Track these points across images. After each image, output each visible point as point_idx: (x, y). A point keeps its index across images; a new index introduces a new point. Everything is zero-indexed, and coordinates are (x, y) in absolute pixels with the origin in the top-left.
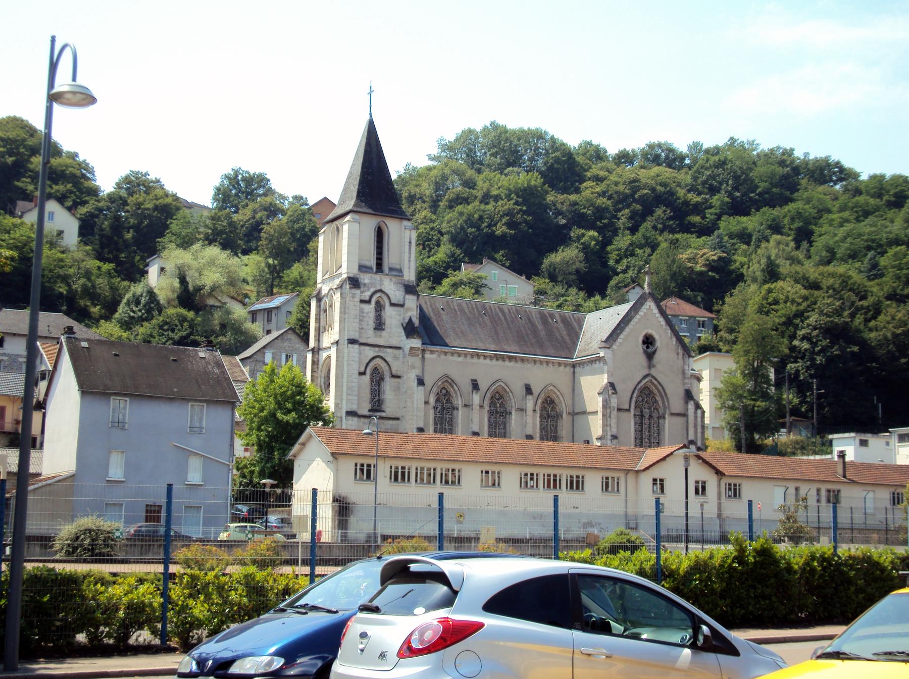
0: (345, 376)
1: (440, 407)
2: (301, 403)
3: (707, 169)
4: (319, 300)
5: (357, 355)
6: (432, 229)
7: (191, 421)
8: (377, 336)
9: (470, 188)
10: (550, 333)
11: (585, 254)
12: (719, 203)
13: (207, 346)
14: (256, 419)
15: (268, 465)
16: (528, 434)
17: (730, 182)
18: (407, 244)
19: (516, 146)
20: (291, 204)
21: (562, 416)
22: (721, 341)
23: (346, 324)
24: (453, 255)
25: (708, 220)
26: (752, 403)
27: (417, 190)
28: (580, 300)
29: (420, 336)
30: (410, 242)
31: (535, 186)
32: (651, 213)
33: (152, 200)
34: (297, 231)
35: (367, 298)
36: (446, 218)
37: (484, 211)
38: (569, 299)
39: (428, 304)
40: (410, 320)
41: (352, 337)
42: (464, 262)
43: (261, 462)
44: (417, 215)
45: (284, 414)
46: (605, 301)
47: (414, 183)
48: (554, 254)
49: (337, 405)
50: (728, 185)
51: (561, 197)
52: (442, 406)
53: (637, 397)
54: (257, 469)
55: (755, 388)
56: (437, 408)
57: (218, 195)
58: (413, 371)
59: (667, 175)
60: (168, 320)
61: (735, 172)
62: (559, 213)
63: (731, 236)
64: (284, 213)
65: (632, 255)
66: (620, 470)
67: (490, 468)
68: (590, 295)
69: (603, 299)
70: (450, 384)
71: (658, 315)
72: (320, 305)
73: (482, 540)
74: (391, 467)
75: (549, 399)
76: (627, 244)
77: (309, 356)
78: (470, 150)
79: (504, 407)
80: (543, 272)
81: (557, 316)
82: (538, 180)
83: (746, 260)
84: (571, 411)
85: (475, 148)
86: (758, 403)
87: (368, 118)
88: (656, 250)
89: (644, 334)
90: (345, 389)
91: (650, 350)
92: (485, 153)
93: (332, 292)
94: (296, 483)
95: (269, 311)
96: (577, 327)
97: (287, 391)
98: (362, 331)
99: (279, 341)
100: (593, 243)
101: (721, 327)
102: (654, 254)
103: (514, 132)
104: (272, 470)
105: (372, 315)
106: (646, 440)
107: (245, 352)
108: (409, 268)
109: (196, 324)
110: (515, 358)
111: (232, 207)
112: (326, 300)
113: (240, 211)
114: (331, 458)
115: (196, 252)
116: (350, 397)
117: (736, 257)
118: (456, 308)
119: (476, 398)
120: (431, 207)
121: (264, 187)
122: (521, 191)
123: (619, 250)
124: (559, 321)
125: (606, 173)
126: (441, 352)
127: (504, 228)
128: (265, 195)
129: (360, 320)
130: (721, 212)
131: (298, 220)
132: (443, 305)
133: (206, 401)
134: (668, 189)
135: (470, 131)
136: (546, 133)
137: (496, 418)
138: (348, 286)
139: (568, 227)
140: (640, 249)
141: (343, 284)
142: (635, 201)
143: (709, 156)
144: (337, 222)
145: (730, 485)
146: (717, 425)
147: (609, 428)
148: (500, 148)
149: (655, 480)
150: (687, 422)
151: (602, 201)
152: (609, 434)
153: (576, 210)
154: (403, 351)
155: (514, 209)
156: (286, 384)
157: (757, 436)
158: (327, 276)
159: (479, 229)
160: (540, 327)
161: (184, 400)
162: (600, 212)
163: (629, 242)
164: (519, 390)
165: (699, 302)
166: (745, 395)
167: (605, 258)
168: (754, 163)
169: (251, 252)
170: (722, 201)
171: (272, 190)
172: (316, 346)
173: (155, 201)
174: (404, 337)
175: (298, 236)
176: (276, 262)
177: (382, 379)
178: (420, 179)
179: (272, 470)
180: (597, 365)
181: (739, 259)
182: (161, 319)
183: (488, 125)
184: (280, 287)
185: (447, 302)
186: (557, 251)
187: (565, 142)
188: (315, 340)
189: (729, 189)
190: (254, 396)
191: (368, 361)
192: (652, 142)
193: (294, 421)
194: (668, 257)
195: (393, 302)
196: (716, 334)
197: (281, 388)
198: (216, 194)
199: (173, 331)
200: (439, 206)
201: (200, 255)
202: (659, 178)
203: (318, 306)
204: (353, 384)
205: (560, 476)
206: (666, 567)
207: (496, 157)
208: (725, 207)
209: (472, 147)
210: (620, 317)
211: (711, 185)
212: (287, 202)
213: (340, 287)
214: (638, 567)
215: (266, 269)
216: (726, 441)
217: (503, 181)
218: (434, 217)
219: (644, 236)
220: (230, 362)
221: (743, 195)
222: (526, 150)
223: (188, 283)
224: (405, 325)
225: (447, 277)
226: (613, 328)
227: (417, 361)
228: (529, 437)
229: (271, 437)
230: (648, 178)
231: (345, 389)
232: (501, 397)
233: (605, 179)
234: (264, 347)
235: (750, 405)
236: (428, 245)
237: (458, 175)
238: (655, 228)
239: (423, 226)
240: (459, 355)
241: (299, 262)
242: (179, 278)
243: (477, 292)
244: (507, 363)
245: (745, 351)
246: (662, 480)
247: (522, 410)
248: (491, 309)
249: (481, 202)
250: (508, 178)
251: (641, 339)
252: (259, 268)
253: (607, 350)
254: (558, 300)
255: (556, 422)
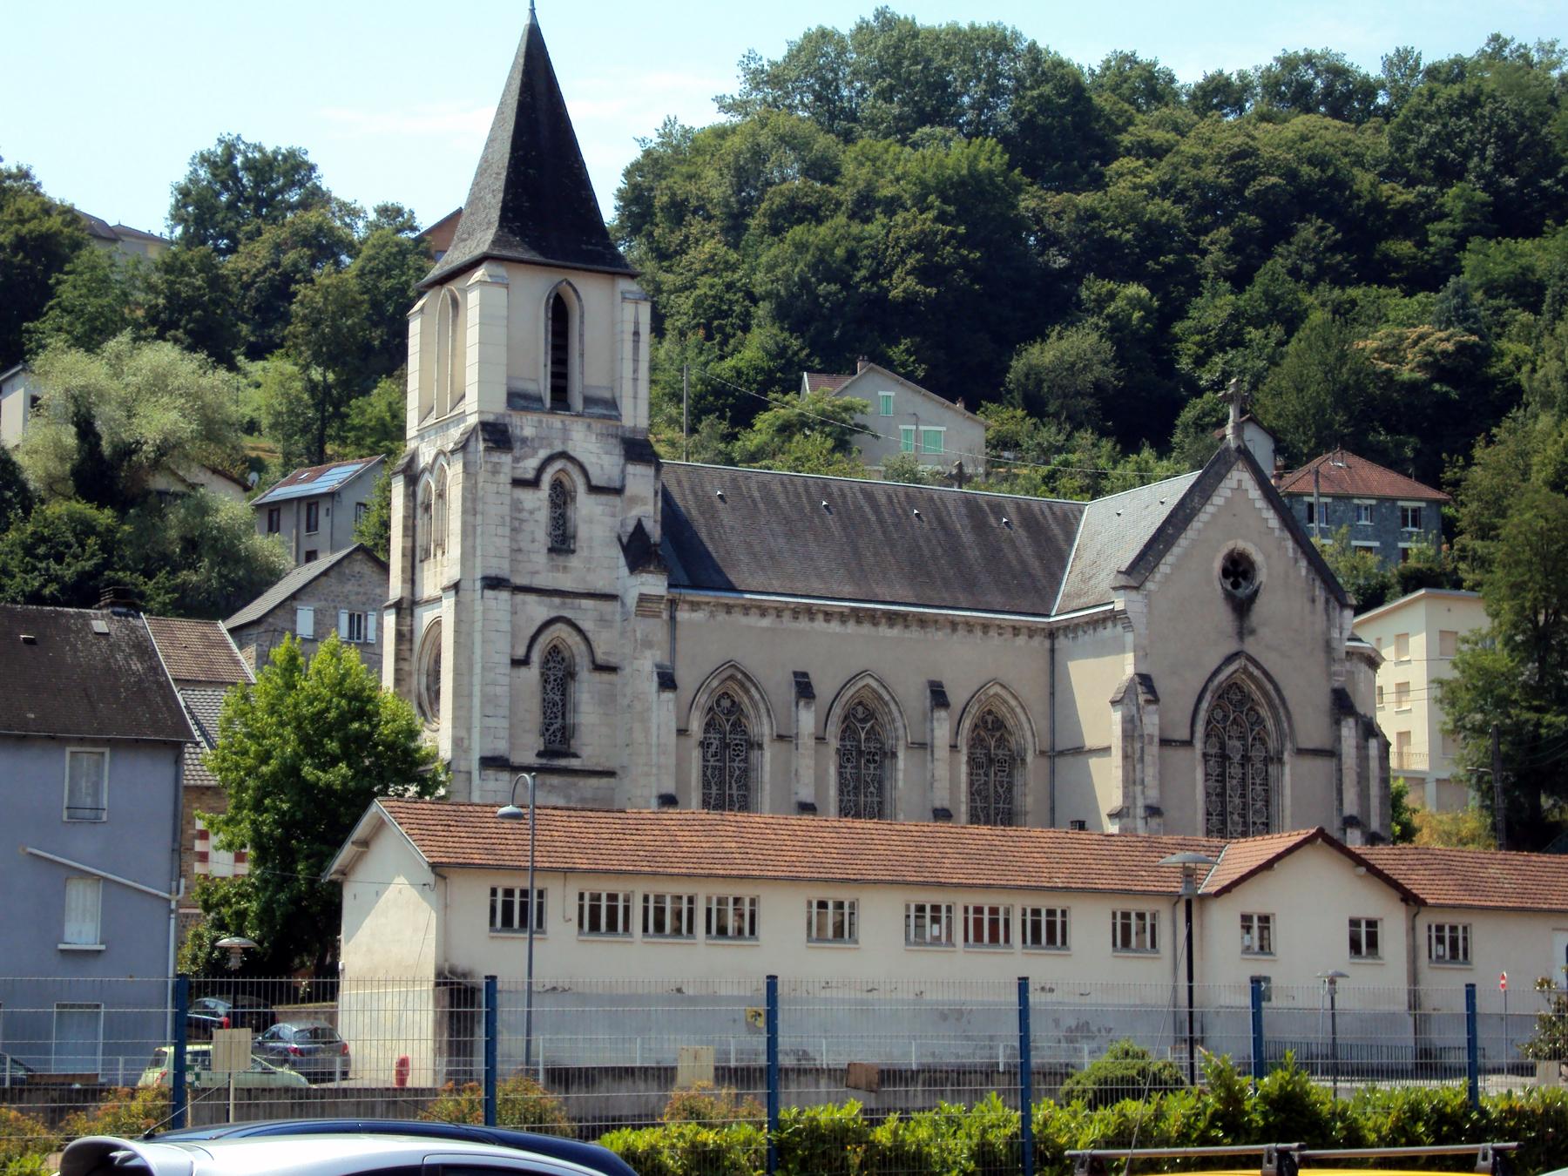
0: (478, 669)
1: (716, 743)
2: (363, 740)
3: (1429, 118)
4: (412, 478)
5: (507, 617)
6: (730, 286)
7: (71, 792)
8: (555, 568)
9: (824, 181)
10: (993, 555)
11: (1119, 344)
12: (1461, 204)
13: (112, 604)
14: (251, 782)
15: (282, 897)
16: (938, 805)
17: (1490, 151)
18: (629, 338)
19: (939, 70)
20: (373, 227)
21: (1023, 760)
22: (1463, 558)
23: (478, 541)
24: (782, 351)
25: (1432, 250)
26: (1532, 716)
27: (691, 187)
28: (1102, 462)
29: (663, 567)
30: (636, 334)
31: (990, 173)
32: (1287, 235)
33: (10, 223)
34: (388, 296)
35: (530, 475)
36: (764, 259)
37: (860, 240)
38: (1073, 458)
39: (686, 485)
40: (639, 526)
41: (492, 573)
42: (810, 370)
43: (265, 889)
44: (692, 252)
45: (323, 767)
46: (1165, 463)
47: (684, 169)
48: (1038, 346)
49: (457, 743)
50: (1483, 159)
51: (1055, 200)
52: (723, 740)
53: (1211, 711)
54: (254, 906)
55: (1541, 679)
56: (710, 745)
57: (185, 206)
58: (648, 653)
59: (1329, 135)
60: (46, 532)
61: (1503, 126)
62: (1050, 240)
63: (1491, 290)
64: (352, 249)
65: (1238, 343)
66: (1158, 894)
67: (831, 895)
68: (1128, 446)
69: (1160, 458)
70: (742, 686)
71: (1261, 504)
72: (414, 495)
73: (682, 1078)
74: (581, 896)
75: (990, 719)
76: (1224, 315)
77: (390, 620)
78: (825, 84)
79: (878, 740)
80: (1009, 392)
81: (1011, 509)
82: (997, 157)
83: (1529, 350)
84: (1046, 747)
85: (835, 79)
86: (1548, 718)
87: (525, 21)
88: (1296, 329)
89: (1224, 551)
90: (477, 701)
91: (1242, 592)
92: (862, 91)
93: (442, 460)
94: (348, 941)
95: (311, 503)
96: (1061, 537)
97: (327, 710)
98: (520, 557)
99: (333, 579)
100: (1137, 315)
101: (1461, 525)
102: (1294, 341)
103: (935, 36)
104: (292, 908)
105: (544, 515)
106: (1236, 817)
107: (245, 610)
108: (635, 397)
109: (120, 542)
110: (905, 616)
111: (221, 236)
112: (429, 480)
113: (241, 248)
114: (430, 877)
115: (118, 357)
116: (491, 722)
117: (1504, 344)
118: (756, 494)
119: (807, 720)
120: (725, 231)
121: (301, 185)
122: (952, 185)
123: (1204, 330)
124: (1016, 522)
125: (1171, 136)
126: (717, 605)
127: (911, 281)
128: (304, 205)
129: (513, 530)
130: (1465, 229)
131: (389, 269)
132: (723, 487)
133: (109, 743)
134: (1330, 172)
135: (824, 35)
136: (1017, 36)
137: (857, 767)
138: (481, 446)
139: (1072, 275)
140: (1256, 328)
141: (468, 440)
142: (1247, 205)
143: (1436, 85)
144: (453, 286)
145: (1440, 928)
146: (1445, 775)
147: (1138, 788)
148: (899, 78)
149: (1246, 919)
150: (1340, 770)
151: (1162, 209)
152: (1140, 803)
153: (1093, 231)
154: (623, 604)
155: (936, 234)
156: (325, 692)
157: (1546, 802)
158: (430, 421)
159: (846, 284)
160: (967, 537)
161: (56, 739)
162: (1155, 235)
163: (1229, 310)
164: (912, 694)
165: (1406, 460)
166: (1515, 696)
167: (1168, 352)
168: (1553, 100)
169: (271, 353)
170: (1468, 201)
171: (324, 194)
172: (407, 594)
173: (16, 226)
174: (624, 571)
175: (391, 309)
176: (331, 377)
177: (571, 675)
178: (700, 160)
179: (292, 908)
180: (1108, 632)
181: (1513, 347)
182: (30, 528)
183: (870, 17)
184: (343, 441)
185: (734, 480)
186: (1045, 338)
187: (1065, 56)
188: (404, 581)
189: (1488, 168)
190: (246, 725)
191: (533, 629)
192: (1291, 51)
193: (344, 784)
194: (1328, 346)
195: (594, 482)
196: (1450, 541)
197: (311, 703)
198: (179, 206)
199: (59, 559)
200: (747, 227)
201: (129, 365)
202: (1307, 145)
203: (411, 495)
204: (499, 690)
205: (1007, 912)
206: (1047, 1140)
207: (891, 101)
208: (1477, 216)
209: (830, 76)
210: (1165, 512)
211: (1441, 160)
212: (361, 224)
213: (463, 447)
214: (975, 1140)
215: (306, 396)
216: (1471, 816)
217: (907, 161)
218: (733, 256)
219: (1266, 293)
220: (204, 636)
221: (1523, 184)
222: (965, 82)
223: (98, 437)
224: (625, 540)
225: (767, 409)
226: (1147, 538)
227: (656, 628)
228: (942, 814)
229: (286, 823)
230: (1279, 146)
231: (477, 701)
232: (870, 715)
233: (1167, 151)
234: (294, 596)
235: (1527, 721)
236: (721, 329)
237: (793, 149)
238: (1295, 273)
239: (706, 279)
240: (763, 611)
241: (389, 375)
242: (77, 425)
243: (842, 445)
244: (884, 630)
245: (1512, 586)
246: (1265, 919)
247: (923, 746)
248: (843, 495)
249: (851, 217)
250: (918, 155)
251: (1217, 565)
252: (286, 394)
253: (1133, 595)
254: (1047, 463)
255: (1010, 775)
